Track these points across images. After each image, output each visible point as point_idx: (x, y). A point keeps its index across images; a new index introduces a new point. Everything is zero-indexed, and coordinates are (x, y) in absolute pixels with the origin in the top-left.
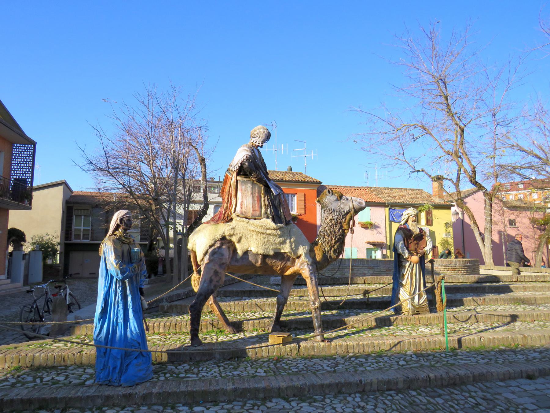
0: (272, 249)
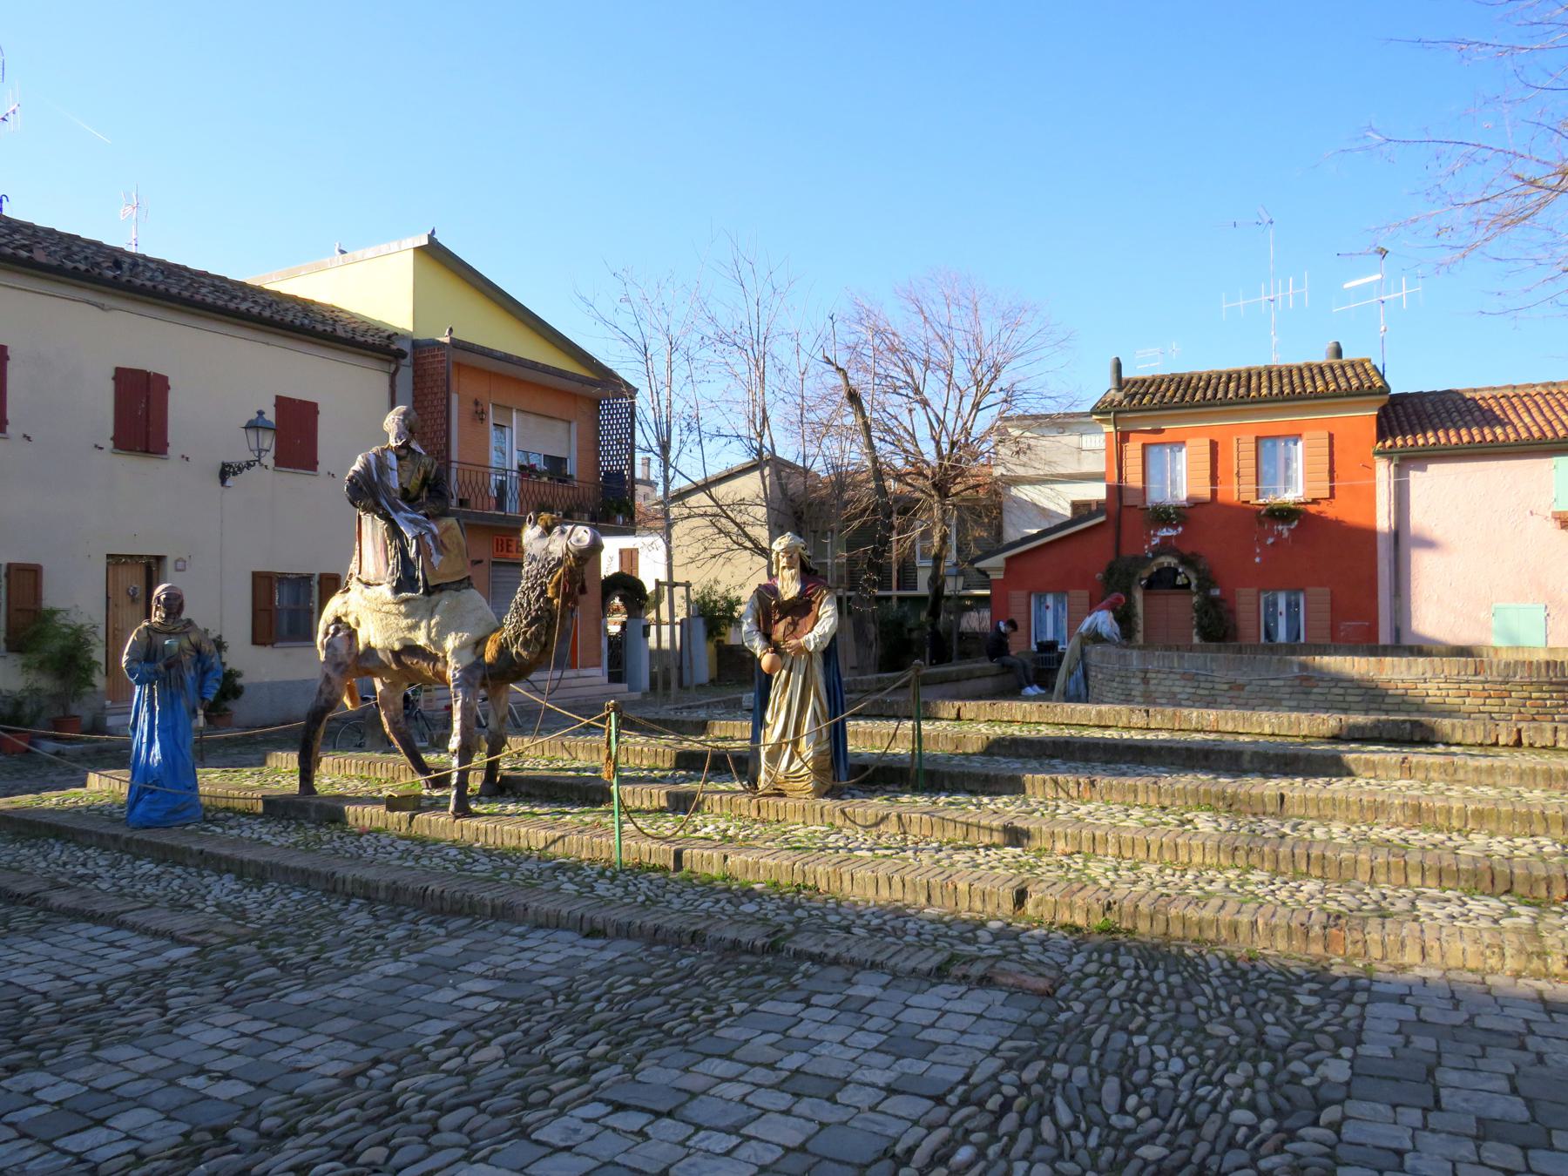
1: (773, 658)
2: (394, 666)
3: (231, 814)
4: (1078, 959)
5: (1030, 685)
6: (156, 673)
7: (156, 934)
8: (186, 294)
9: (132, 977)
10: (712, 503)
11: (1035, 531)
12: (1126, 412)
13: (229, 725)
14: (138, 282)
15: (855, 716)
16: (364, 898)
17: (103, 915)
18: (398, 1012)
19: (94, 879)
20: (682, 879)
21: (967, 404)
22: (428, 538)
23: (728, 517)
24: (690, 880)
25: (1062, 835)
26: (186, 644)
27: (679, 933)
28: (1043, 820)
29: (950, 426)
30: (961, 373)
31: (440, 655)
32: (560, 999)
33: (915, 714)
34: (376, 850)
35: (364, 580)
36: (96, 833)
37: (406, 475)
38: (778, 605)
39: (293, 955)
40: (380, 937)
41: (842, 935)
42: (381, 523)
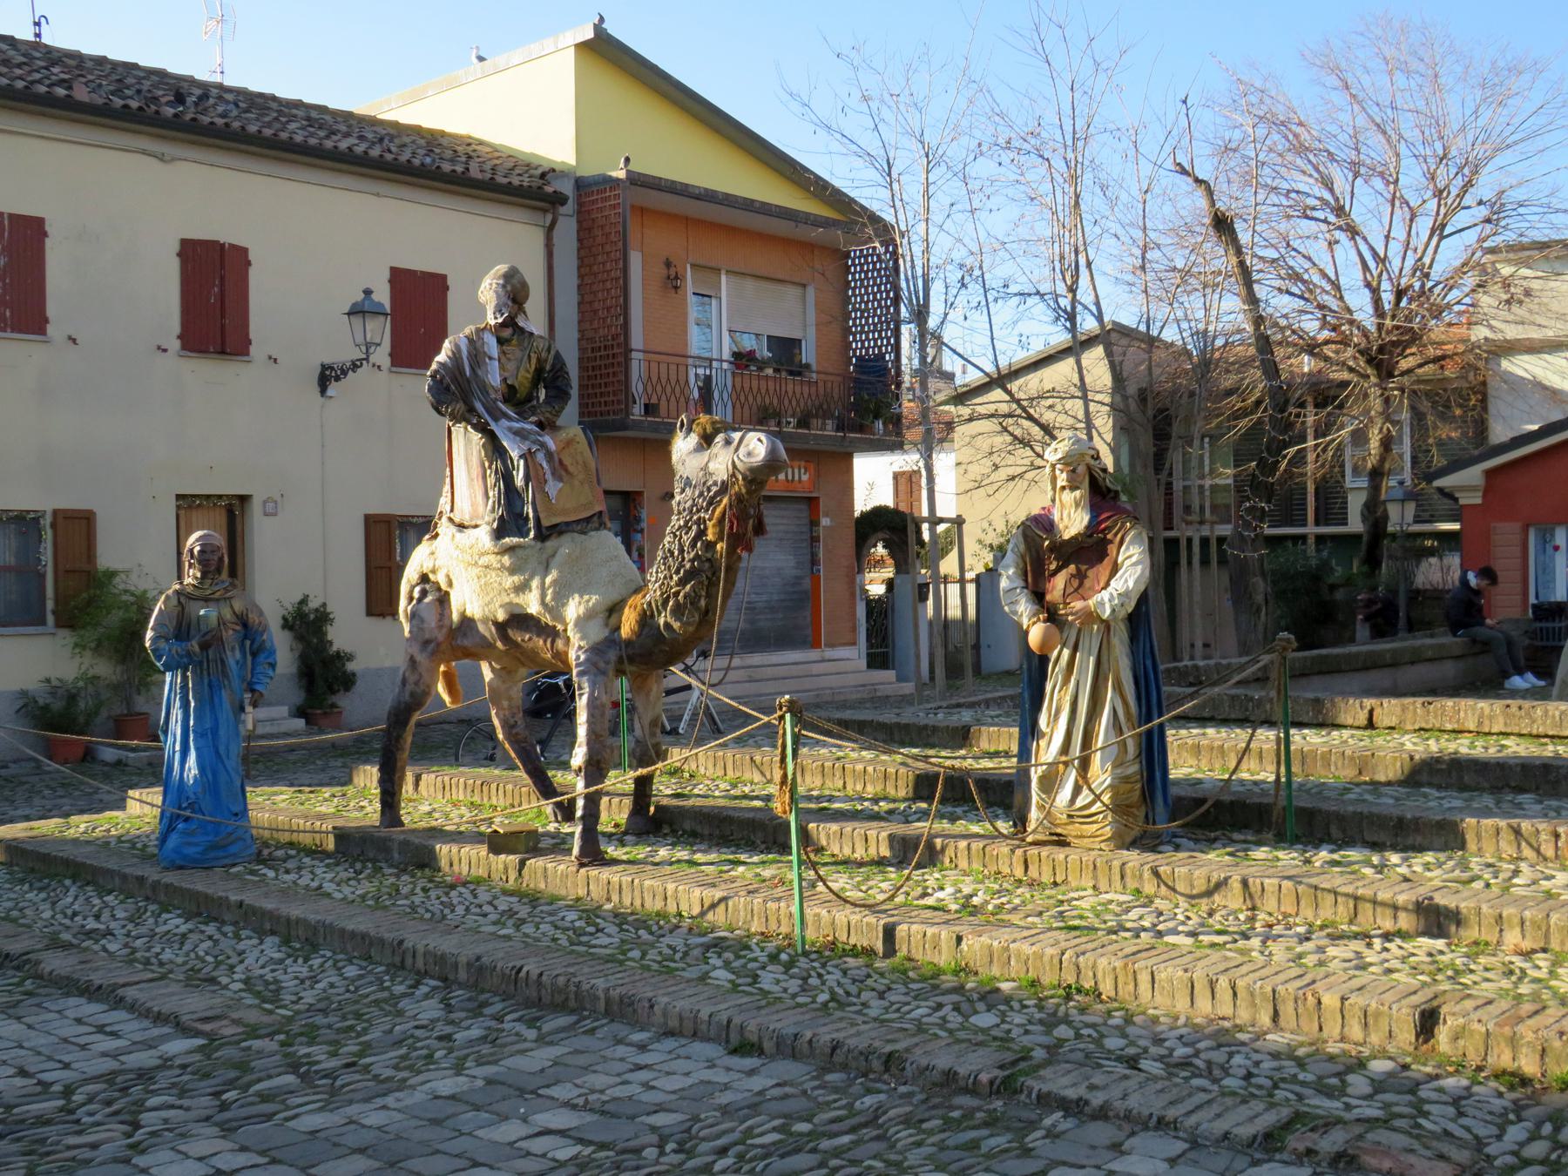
1: (1047, 629)
2: (499, 644)
3: (293, 852)
4: (1515, 1133)
5: (1520, 673)
6: (189, 654)
7: (159, 1018)
8: (268, 132)
9: (109, 1078)
10: (1007, 398)
11: (1536, 427)
13: (339, 728)
14: (206, 120)
15: (1185, 720)
16: (439, 979)
17: (100, 987)
18: (437, 1152)
19: (104, 936)
20: (894, 970)
21: (1424, 225)
22: (540, 457)
23: (1030, 418)
24: (904, 972)
25: (1516, 920)
26: (228, 615)
27: (866, 1054)
28: (1487, 895)
29: (1396, 263)
30: (1412, 179)
31: (560, 627)
32: (670, 1147)
33: (1278, 715)
34: (467, 909)
35: (457, 520)
37: (511, 366)
38: (1052, 548)
39: (323, 1057)
40: (447, 1038)
41: (1121, 1069)
42: (476, 438)
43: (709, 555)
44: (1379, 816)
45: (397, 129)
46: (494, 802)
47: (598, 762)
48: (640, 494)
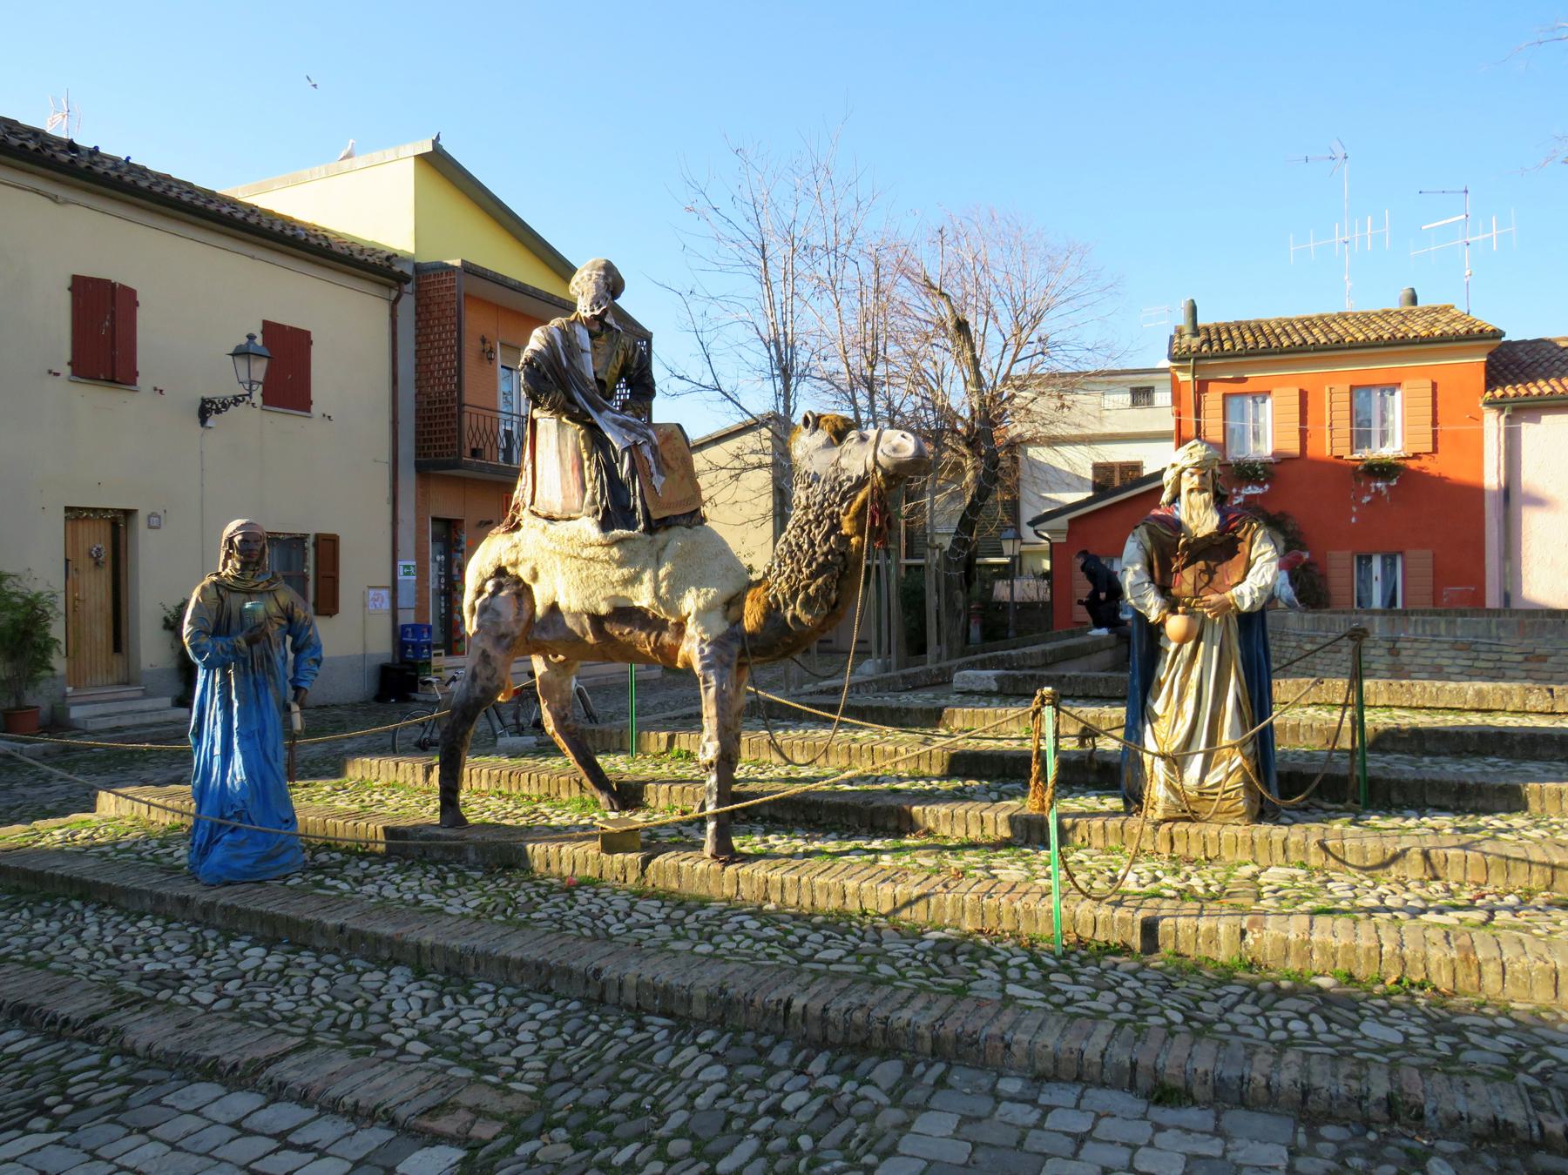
0: (604, 599)
2: (590, 638)
6: (235, 650)
12: (1207, 358)
17: (235, 1067)
26: (274, 609)
35: (542, 512)
36: (150, 893)
42: (573, 430)
43: (842, 549)
44: (1440, 783)
45: (253, 210)
46: (525, 791)
47: (729, 756)
48: (461, 521)
